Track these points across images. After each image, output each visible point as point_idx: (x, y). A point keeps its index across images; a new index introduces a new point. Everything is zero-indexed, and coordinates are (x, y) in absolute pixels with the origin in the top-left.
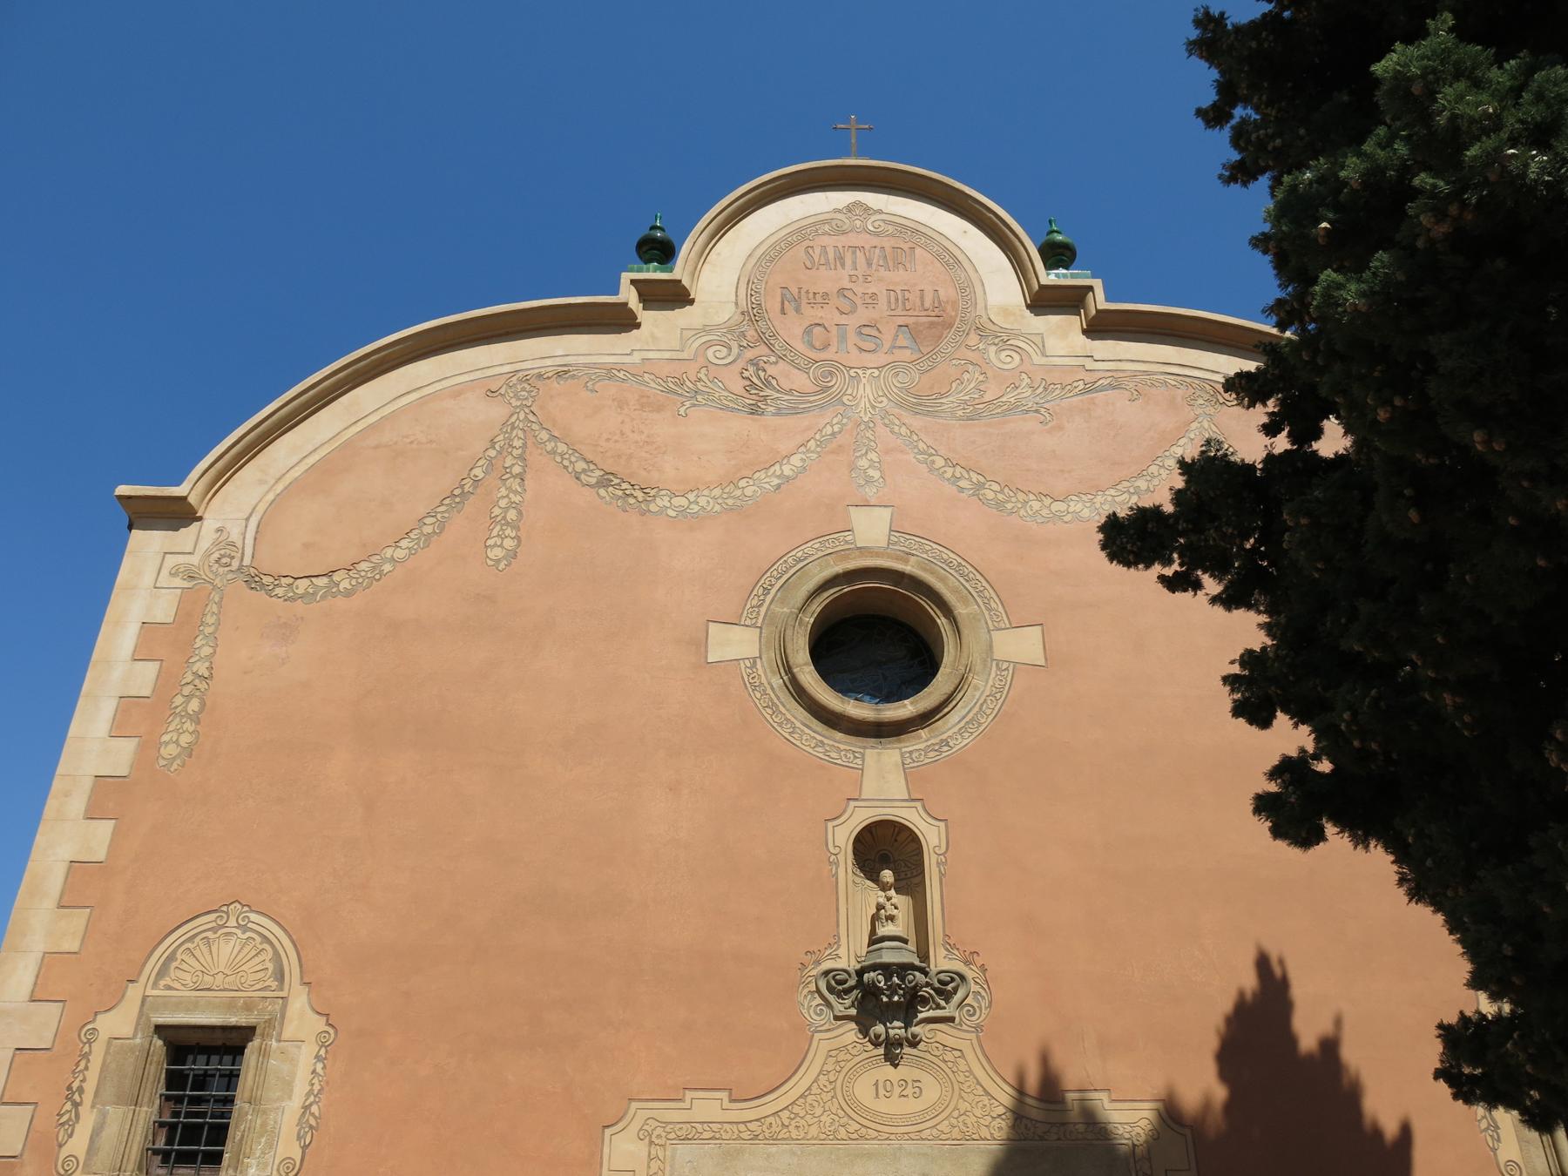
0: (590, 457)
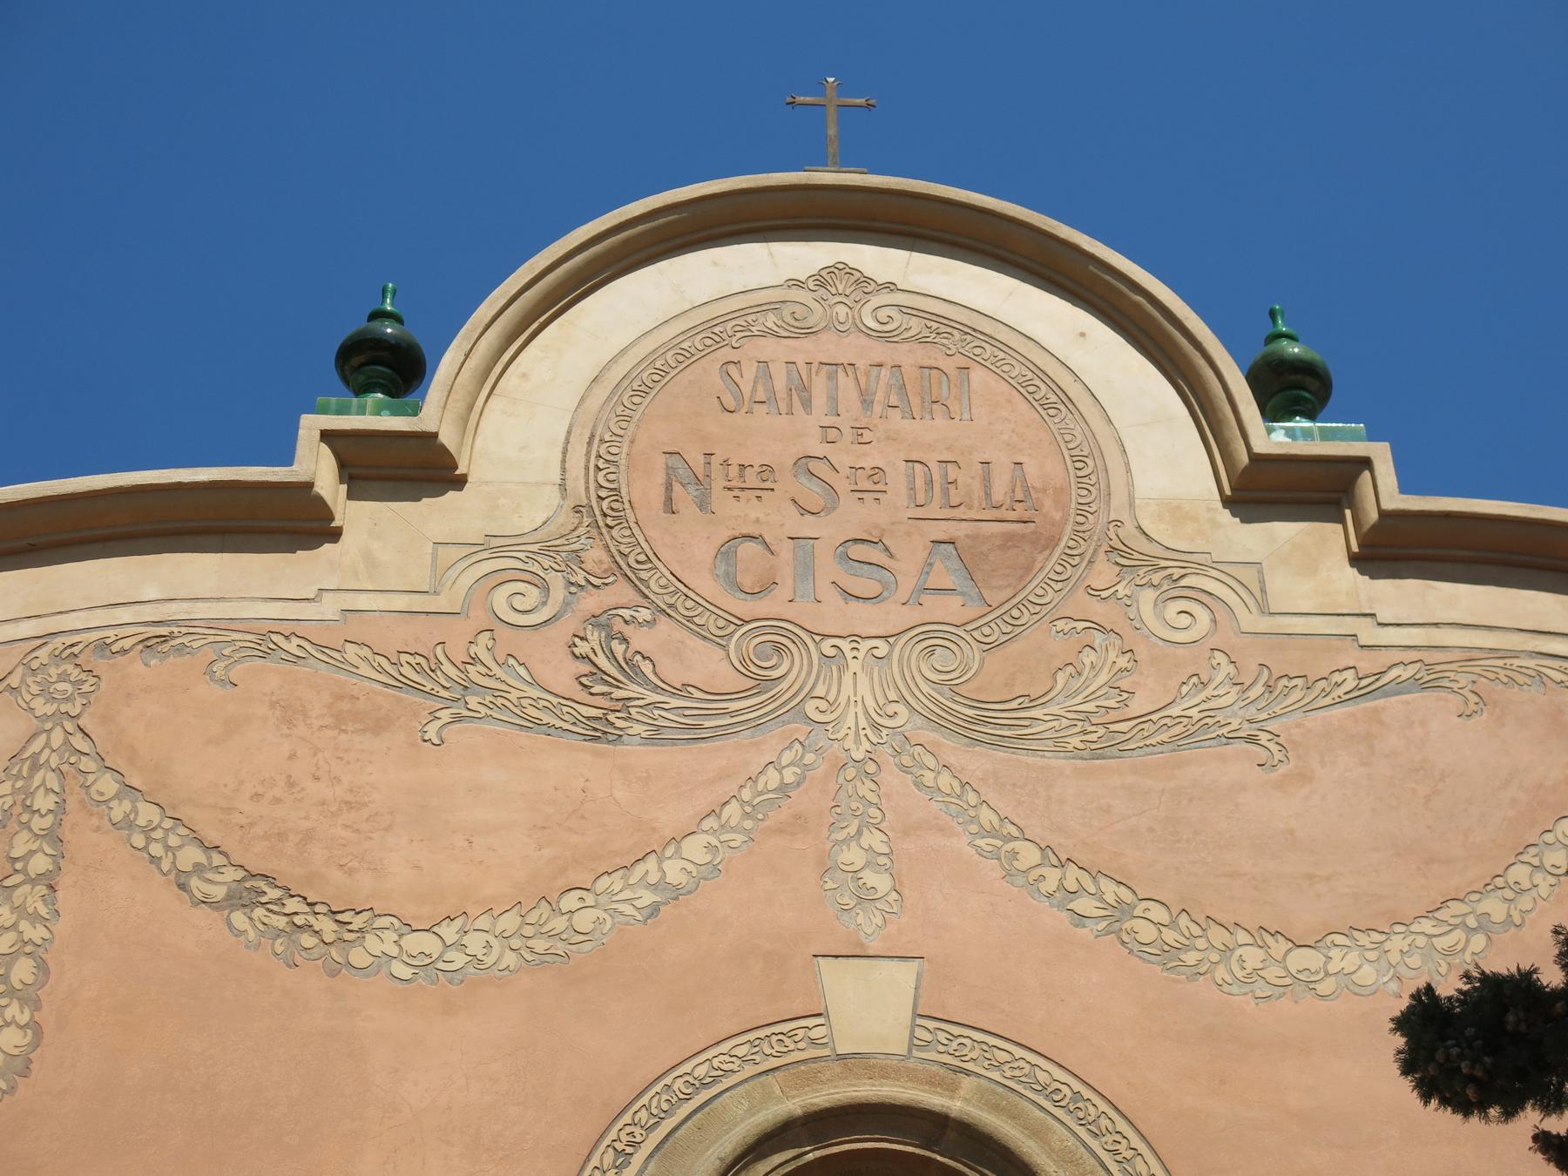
0: (212, 836)
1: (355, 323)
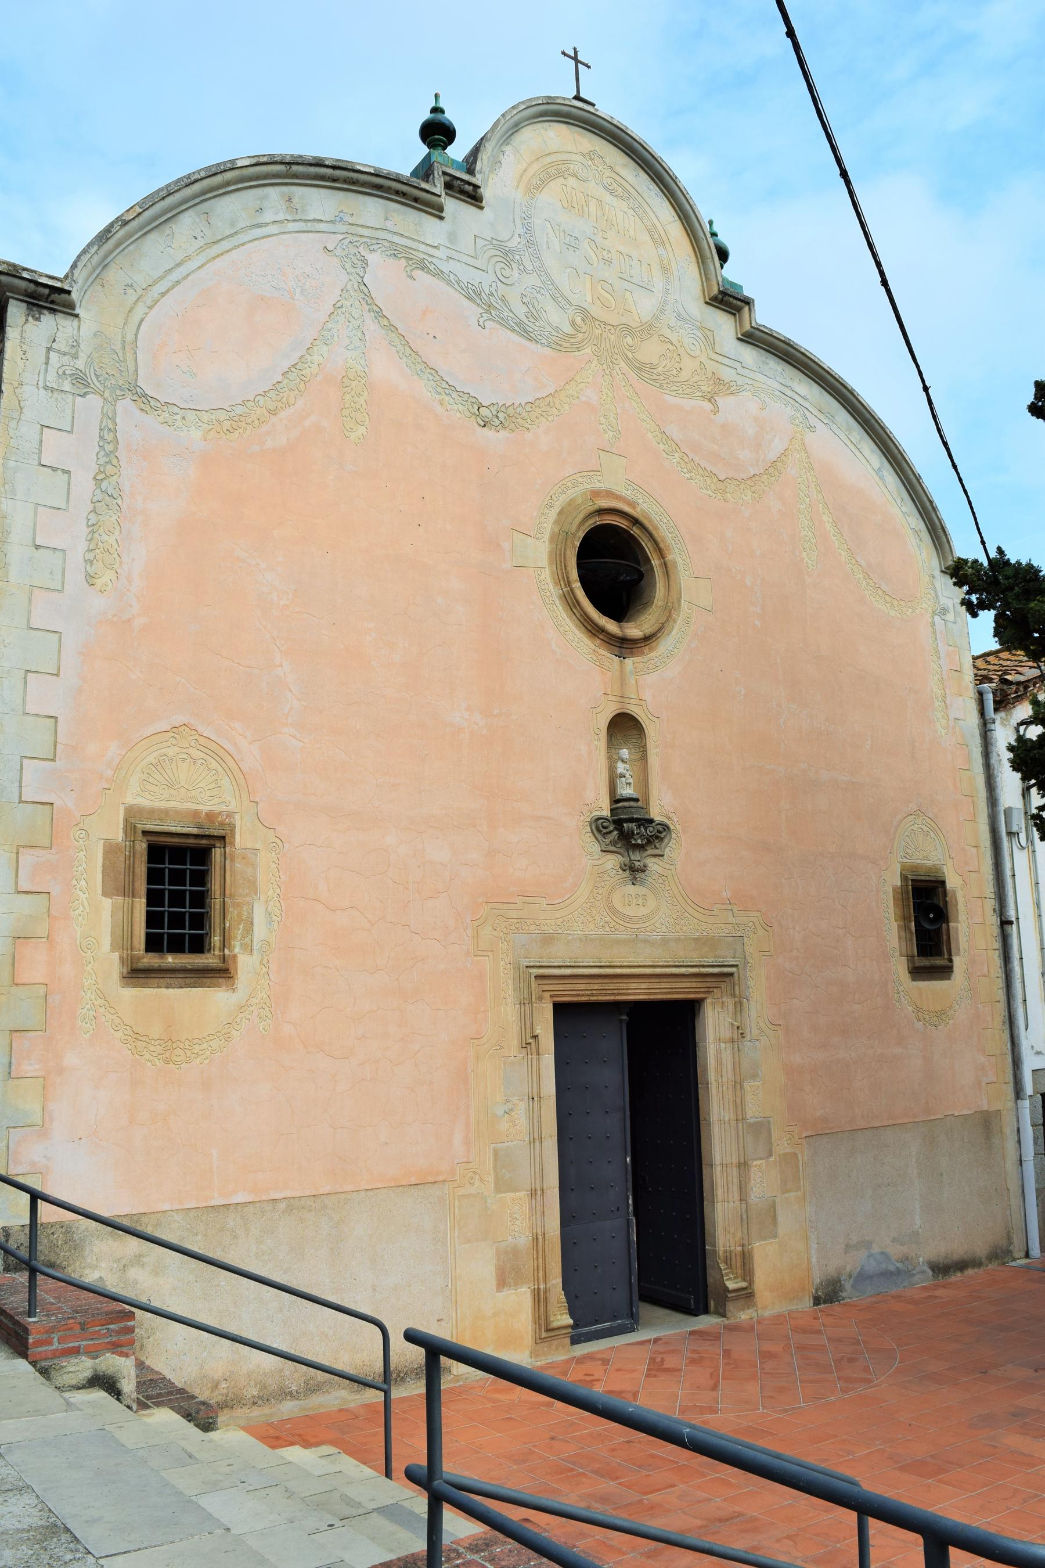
1: (426, 115)
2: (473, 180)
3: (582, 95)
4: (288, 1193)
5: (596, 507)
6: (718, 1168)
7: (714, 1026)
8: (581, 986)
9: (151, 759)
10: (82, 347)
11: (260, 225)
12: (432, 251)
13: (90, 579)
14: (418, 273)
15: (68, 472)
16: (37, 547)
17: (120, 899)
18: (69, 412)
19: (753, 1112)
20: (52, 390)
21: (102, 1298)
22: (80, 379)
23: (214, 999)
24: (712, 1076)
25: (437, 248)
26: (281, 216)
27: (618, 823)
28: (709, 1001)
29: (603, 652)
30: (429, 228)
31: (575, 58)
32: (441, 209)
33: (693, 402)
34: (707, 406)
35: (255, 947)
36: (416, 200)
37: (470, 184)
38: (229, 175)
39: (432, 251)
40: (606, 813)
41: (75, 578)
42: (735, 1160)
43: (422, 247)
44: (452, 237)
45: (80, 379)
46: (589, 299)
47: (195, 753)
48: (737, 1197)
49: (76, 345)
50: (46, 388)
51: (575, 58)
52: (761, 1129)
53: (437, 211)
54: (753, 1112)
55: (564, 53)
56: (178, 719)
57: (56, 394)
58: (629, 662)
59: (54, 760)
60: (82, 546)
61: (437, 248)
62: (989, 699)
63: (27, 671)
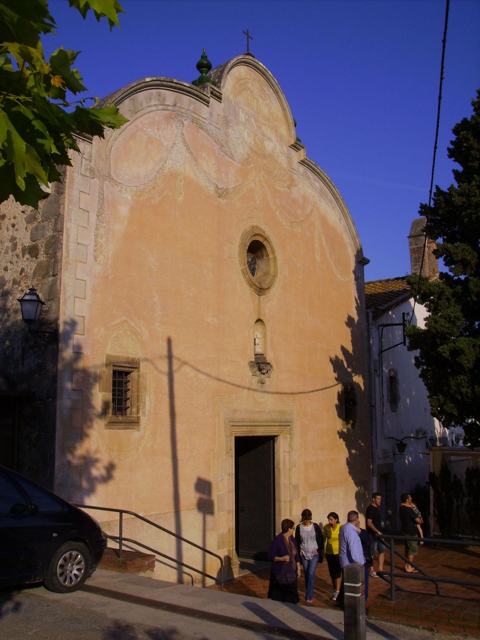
2: (220, 91)
3: (250, 52)
4: (155, 512)
5: (254, 233)
6: (283, 503)
7: (282, 449)
8: (244, 429)
9: (115, 335)
10: (93, 157)
11: (150, 106)
12: (204, 120)
13: (95, 258)
14: (200, 130)
15: (88, 212)
16: (78, 244)
17: (104, 393)
18: (89, 185)
19: (294, 481)
20: (83, 175)
21: (149, 519)
22: (91, 170)
23: (135, 434)
24: (281, 466)
25: (205, 119)
26: (157, 103)
27: (258, 363)
28: (281, 436)
29: (254, 293)
30: (204, 110)
31: (247, 35)
32: (208, 103)
33: (284, 189)
34: (288, 190)
35: (146, 413)
36: (201, 98)
37: (219, 92)
38: (143, 85)
39: (204, 120)
40: (253, 360)
41: (91, 258)
42: (288, 500)
43: (201, 119)
44: (211, 114)
45: (91, 170)
46: (253, 143)
47: (128, 333)
48: (289, 514)
49: (91, 156)
50: (81, 174)
51: (247, 35)
52: (296, 487)
53: (207, 103)
54: (294, 481)
55: (244, 32)
56: (124, 318)
57: (84, 177)
58: (262, 297)
59: (83, 335)
60: (93, 244)
61: (205, 119)
62: (371, 315)
63: (75, 297)
